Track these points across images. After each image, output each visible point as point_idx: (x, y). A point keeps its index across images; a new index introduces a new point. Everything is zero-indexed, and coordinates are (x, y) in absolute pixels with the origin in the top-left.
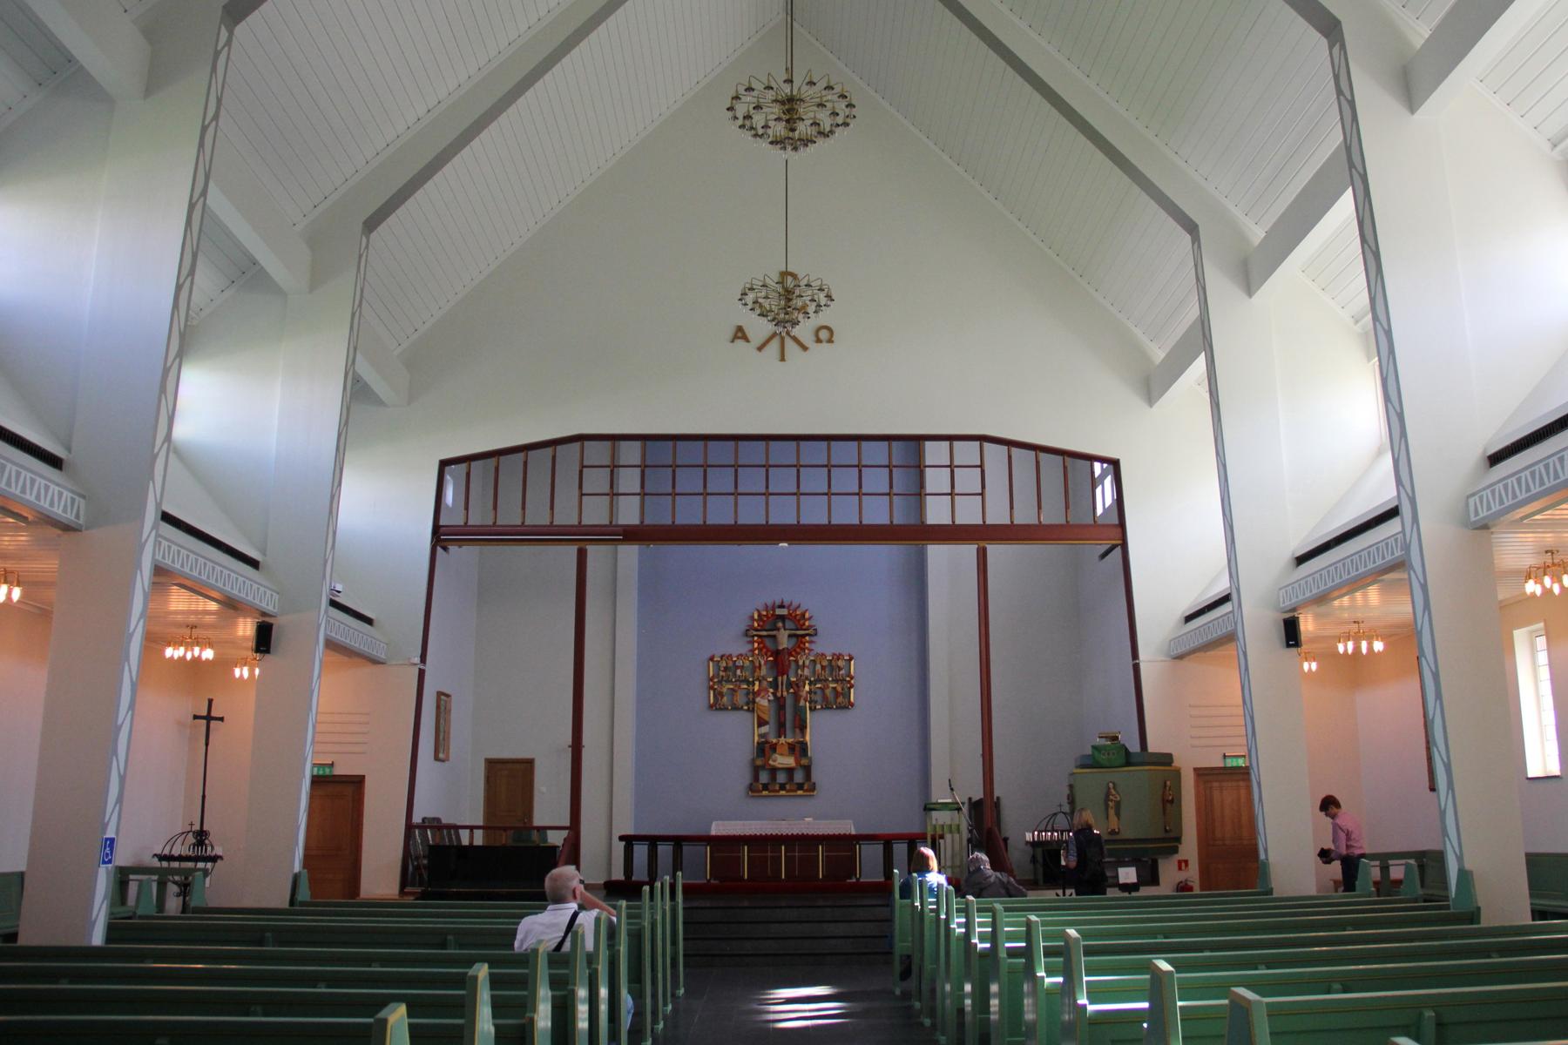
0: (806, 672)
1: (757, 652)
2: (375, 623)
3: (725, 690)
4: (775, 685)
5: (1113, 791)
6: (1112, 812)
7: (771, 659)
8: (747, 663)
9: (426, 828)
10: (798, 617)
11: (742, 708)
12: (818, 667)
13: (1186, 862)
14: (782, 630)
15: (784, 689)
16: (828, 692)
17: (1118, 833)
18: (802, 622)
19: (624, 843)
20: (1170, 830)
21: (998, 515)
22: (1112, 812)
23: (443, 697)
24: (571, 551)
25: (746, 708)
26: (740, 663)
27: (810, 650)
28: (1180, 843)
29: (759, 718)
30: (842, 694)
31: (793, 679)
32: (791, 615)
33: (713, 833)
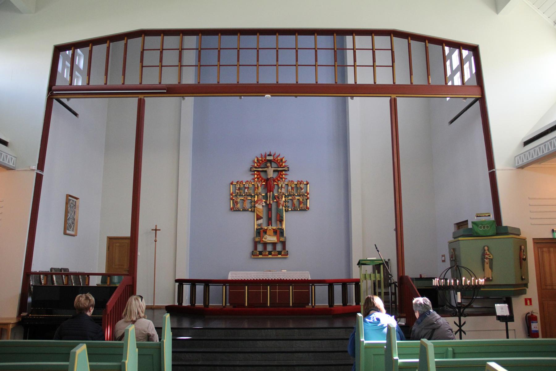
0: (283, 190)
1: (256, 180)
2: (9, 144)
3: (239, 200)
4: (266, 197)
5: (487, 251)
6: (487, 266)
7: (264, 183)
8: (251, 185)
9: (62, 274)
10: (279, 161)
11: (248, 210)
12: (290, 188)
13: (530, 300)
14: (270, 167)
15: (271, 200)
16: (295, 201)
17: (491, 280)
18: (281, 164)
20: (524, 279)
21: (402, 79)
22: (487, 266)
23: (70, 198)
24: (133, 102)
25: (250, 210)
26: (247, 186)
27: (285, 179)
28: (527, 288)
30: (303, 202)
31: (276, 194)
32: (274, 159)
33: (230, 278)
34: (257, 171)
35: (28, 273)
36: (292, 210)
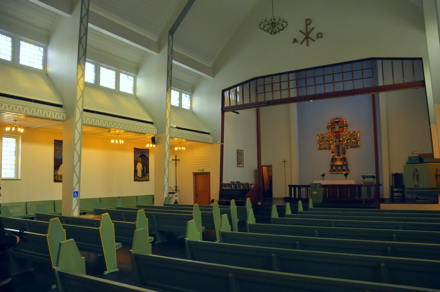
2: (210, 134)
3: (322, 144)
6: (415, 179)
7: (335, 134)
11: (327, 149)
14: (337, 126)
19: (289, 187)
23: (238, 151)
26: (326, 136)
29: (332, 151)
34: (331, 128)
35: (222, 185)
36: (350, 148)
